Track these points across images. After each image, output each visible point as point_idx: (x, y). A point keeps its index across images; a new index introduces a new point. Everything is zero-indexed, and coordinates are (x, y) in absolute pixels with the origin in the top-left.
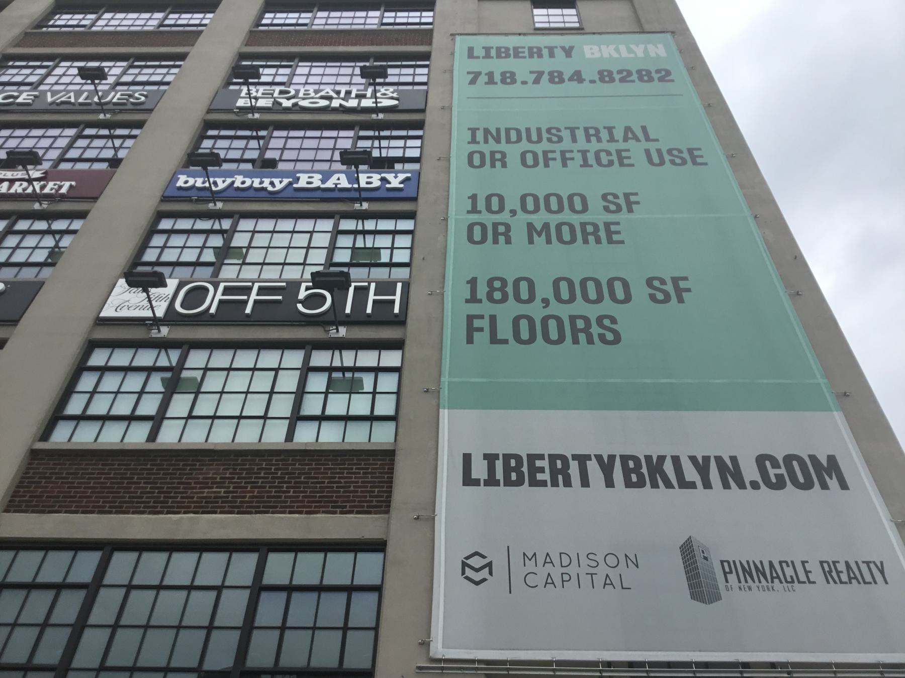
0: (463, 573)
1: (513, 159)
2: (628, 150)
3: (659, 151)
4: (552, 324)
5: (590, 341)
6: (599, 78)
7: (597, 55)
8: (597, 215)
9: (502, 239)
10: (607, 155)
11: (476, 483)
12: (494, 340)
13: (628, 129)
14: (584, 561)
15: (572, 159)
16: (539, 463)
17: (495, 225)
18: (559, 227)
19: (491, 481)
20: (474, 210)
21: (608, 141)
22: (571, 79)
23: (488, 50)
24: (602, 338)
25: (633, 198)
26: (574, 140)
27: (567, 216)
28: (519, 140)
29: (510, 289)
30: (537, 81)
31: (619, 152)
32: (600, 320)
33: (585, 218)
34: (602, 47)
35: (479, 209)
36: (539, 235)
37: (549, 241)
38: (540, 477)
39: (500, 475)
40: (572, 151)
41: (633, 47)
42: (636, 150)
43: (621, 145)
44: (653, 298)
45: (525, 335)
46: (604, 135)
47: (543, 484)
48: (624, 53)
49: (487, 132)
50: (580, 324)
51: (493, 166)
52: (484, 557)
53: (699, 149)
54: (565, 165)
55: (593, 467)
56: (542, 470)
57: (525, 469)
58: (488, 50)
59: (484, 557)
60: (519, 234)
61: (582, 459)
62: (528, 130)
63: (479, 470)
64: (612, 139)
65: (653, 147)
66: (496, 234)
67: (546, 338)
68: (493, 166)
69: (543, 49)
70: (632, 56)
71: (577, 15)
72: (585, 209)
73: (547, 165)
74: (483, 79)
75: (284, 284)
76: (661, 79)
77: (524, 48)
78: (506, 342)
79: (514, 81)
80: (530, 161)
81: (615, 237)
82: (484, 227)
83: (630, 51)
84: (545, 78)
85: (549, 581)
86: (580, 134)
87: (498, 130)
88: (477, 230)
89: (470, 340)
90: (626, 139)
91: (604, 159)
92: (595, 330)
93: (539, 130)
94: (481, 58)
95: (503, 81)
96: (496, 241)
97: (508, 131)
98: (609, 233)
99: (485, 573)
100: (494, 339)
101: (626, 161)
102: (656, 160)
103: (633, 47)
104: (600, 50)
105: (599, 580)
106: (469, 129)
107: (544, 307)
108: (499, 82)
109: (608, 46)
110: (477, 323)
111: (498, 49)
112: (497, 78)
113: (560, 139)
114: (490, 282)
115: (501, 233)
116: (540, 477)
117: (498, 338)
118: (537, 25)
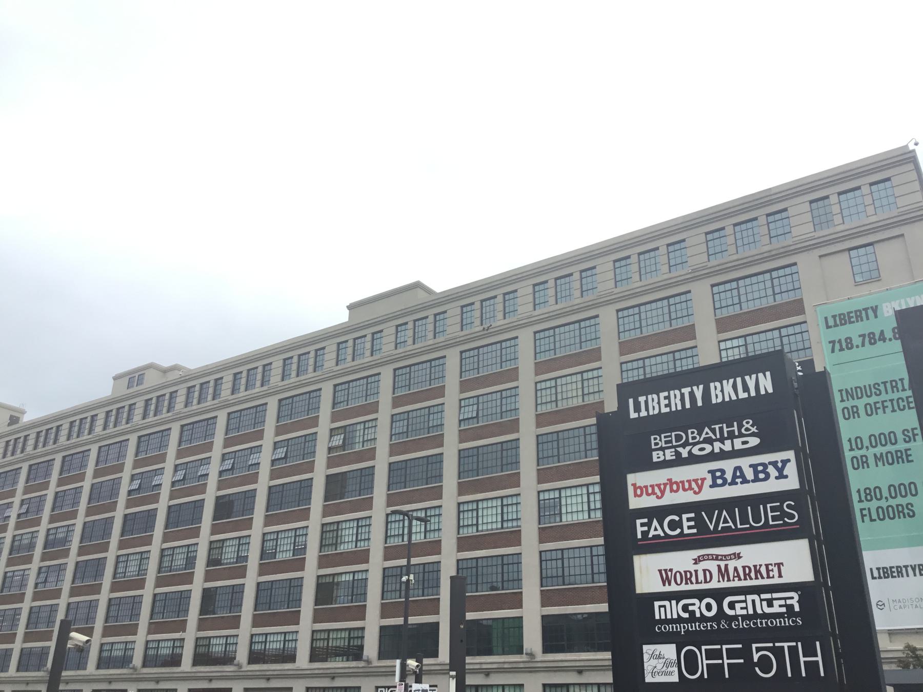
8: (901, 446)
11: (830, 327)
12: (872, 520)
14: (910, 601)
16: (851, 315)
19: (880, 577)
27: (889, 448)
29: (873, 494)
36: (880, 461)
37: (884, 465)
38: (852, 320)
39: (838, 322)
47: (895, 577)
54: (884, 412)
55: (909, 569)
56: (852, 317)
57: (889, 572)
60: (871, 461)
61: (906, 567)
63: (831, 322)
78: (875, 520)
81: (910, 458)
85: (900, 607)
92: (906, 511)
98: (907, 456)
99: (883, 607)
105: (914, 606)
116: (852, 320)
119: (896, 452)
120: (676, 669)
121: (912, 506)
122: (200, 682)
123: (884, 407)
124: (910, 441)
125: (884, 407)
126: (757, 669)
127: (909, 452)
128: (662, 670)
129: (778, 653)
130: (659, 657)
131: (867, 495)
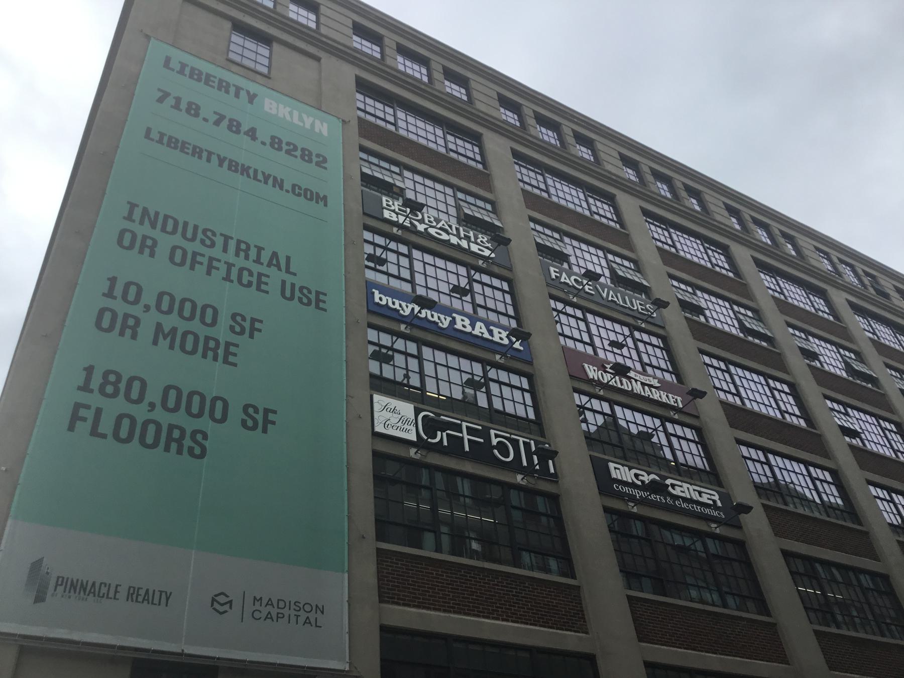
0: (212, 605)
1: (163, 250)
2: (268, 276)
3: (293, 286)
4: (151, 428)
5: (180, 452)
6: (270, 143)
7: (274, 112)
8: (222, 332)
9: (128, 332)
10: (249, 276)
12: (94, 432)
13: (275, 255)
15: (218, 269)
17: (126, 316)
18: (185, 334)
20: (110, 294)
21: (254, 261)
22: (246, 133)
23: (183, 66)
24: (191, 451)
25: (257, 325)
26: (225, 250)
27: (195, 325)
28: (174, 232)
29: (122, 386)
30: (217, 123)
31: (260, 275)
32: (194, 433)
33: (210, 332)
34: (280, 104)
35: (91, 387)
36: (165, 338)
37: (172, 347)
40: (219, 261)
41: (305, 116)
42: (275, 277)
43: (264, 269)
44: (244, 423)
45: (124, 434)
46: (253, 253)
48: (296, 120)
49: (145, 212)
50: (176, 434)
51: (141, 252)
52: (227, 596)
53: (325, 295)
54: (209, 273)
58: (183, 66)
59: (227, 596)
60: (146, 331)
62: (186, 224)
64: (258, 261)
65: (289, 279)
66: (124, 326)
67: (142, 441)
68: (141, 252)
69: (231, 86)
70: (301, 124)
71: (269, 58)
72: (214, 322)
73: (192, 268)
74: (170, 101)
75: (480, 428)
76: (318, 164)
77: (215, 77)
78: (104, 436)
79: (197, 115)
80: (178, 258)
81: (231, 359)
82: (114, 315)
83: (301, 119)
84: (225, 123)
86: (232, 245)
87: (157, 214)
88: (128, 236)
89: (71, 428)
90: (270, 265)
91: (246, 278)
92: (187, 442)
93: (196, 228)
94: (175, 71)
95: (188, 111)
96: (122, 334)
97: (166, 217)
98: (227, 353)
99: (227, 607)
100: (94, 432)
101: (263, 287)
102: (288, 294)
103: (305, 116)
104: (277, 109)
106: (129, 203)
107: (149, 411)
108: (184, 110)
109: (285, 107)
110: (82, 412)
111: (193, 69)
112: (183, 106)
113: (213, 245)
114: (107, 373)
115: (149, 247)
117: (99, 431)
118: (232, 56)
119: (207, 339)
120: (414, 429)
121: (205, 437)
122: (620, 315)
123: (194, 262)
124: (242, 332)
125: (194, 262)
126: (496, 452)
127: (232, 349)
128: (397, 425)
129: (515, 443)
130: (394, 411)
131: (106, 382)
